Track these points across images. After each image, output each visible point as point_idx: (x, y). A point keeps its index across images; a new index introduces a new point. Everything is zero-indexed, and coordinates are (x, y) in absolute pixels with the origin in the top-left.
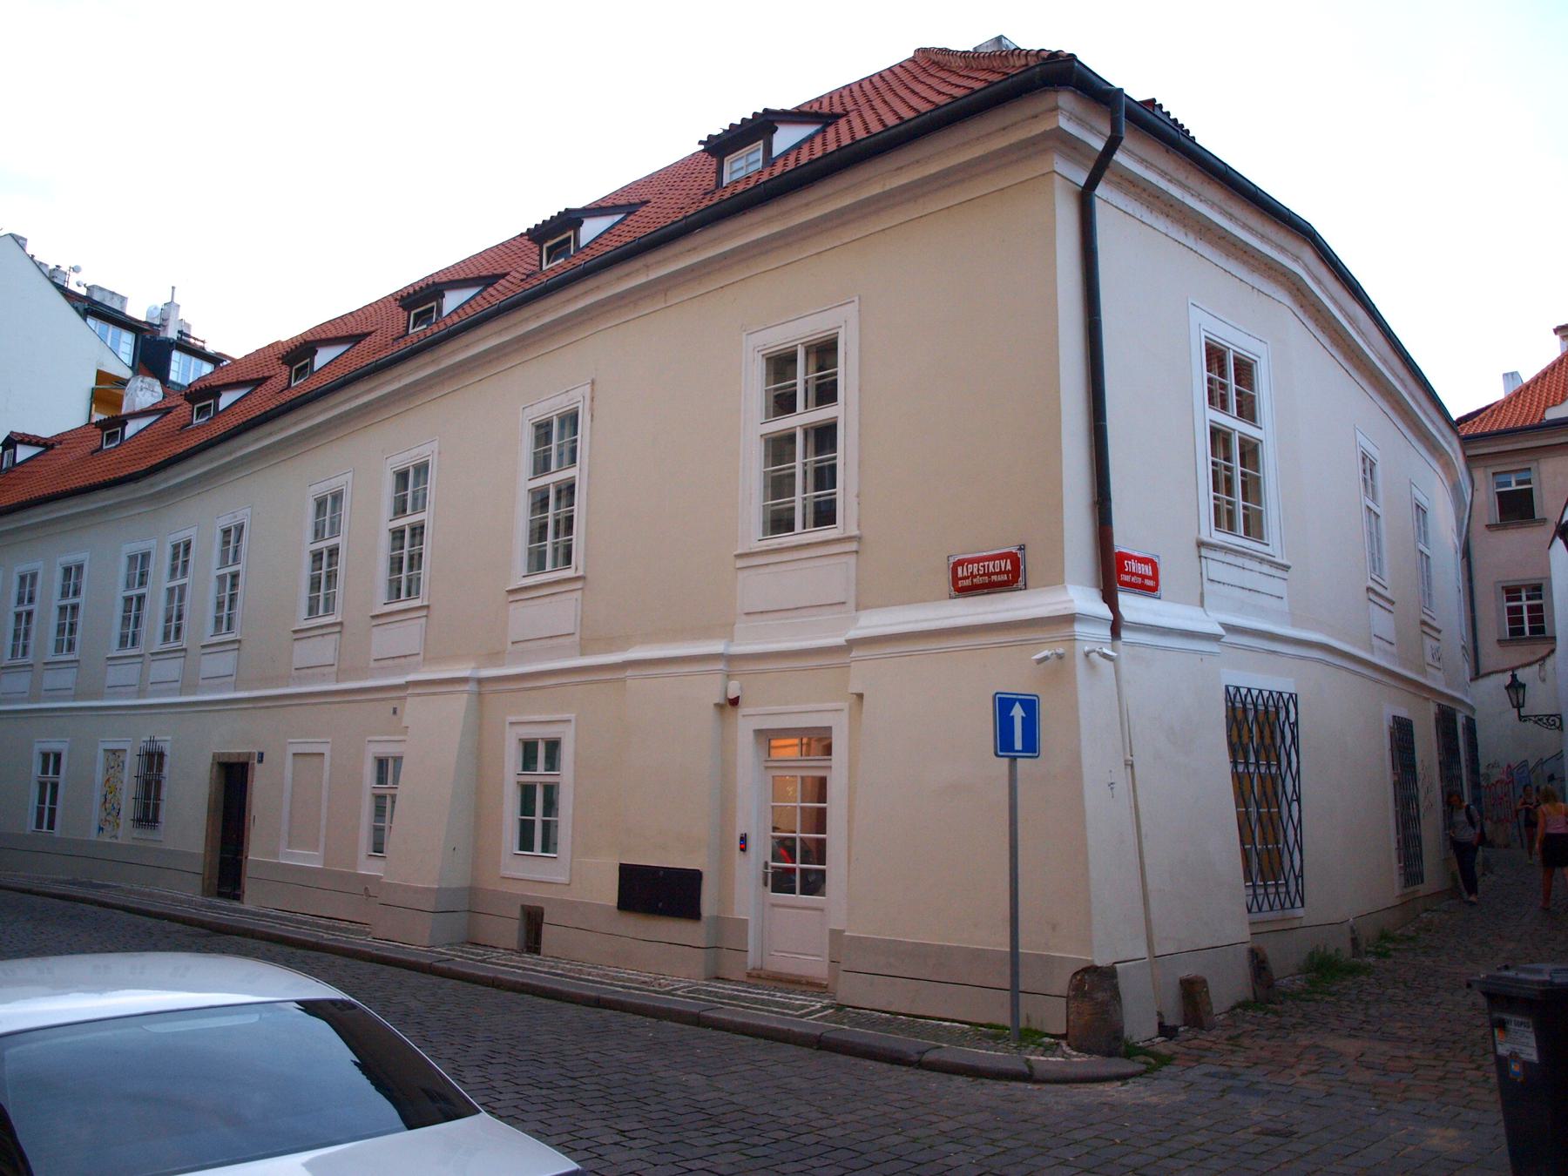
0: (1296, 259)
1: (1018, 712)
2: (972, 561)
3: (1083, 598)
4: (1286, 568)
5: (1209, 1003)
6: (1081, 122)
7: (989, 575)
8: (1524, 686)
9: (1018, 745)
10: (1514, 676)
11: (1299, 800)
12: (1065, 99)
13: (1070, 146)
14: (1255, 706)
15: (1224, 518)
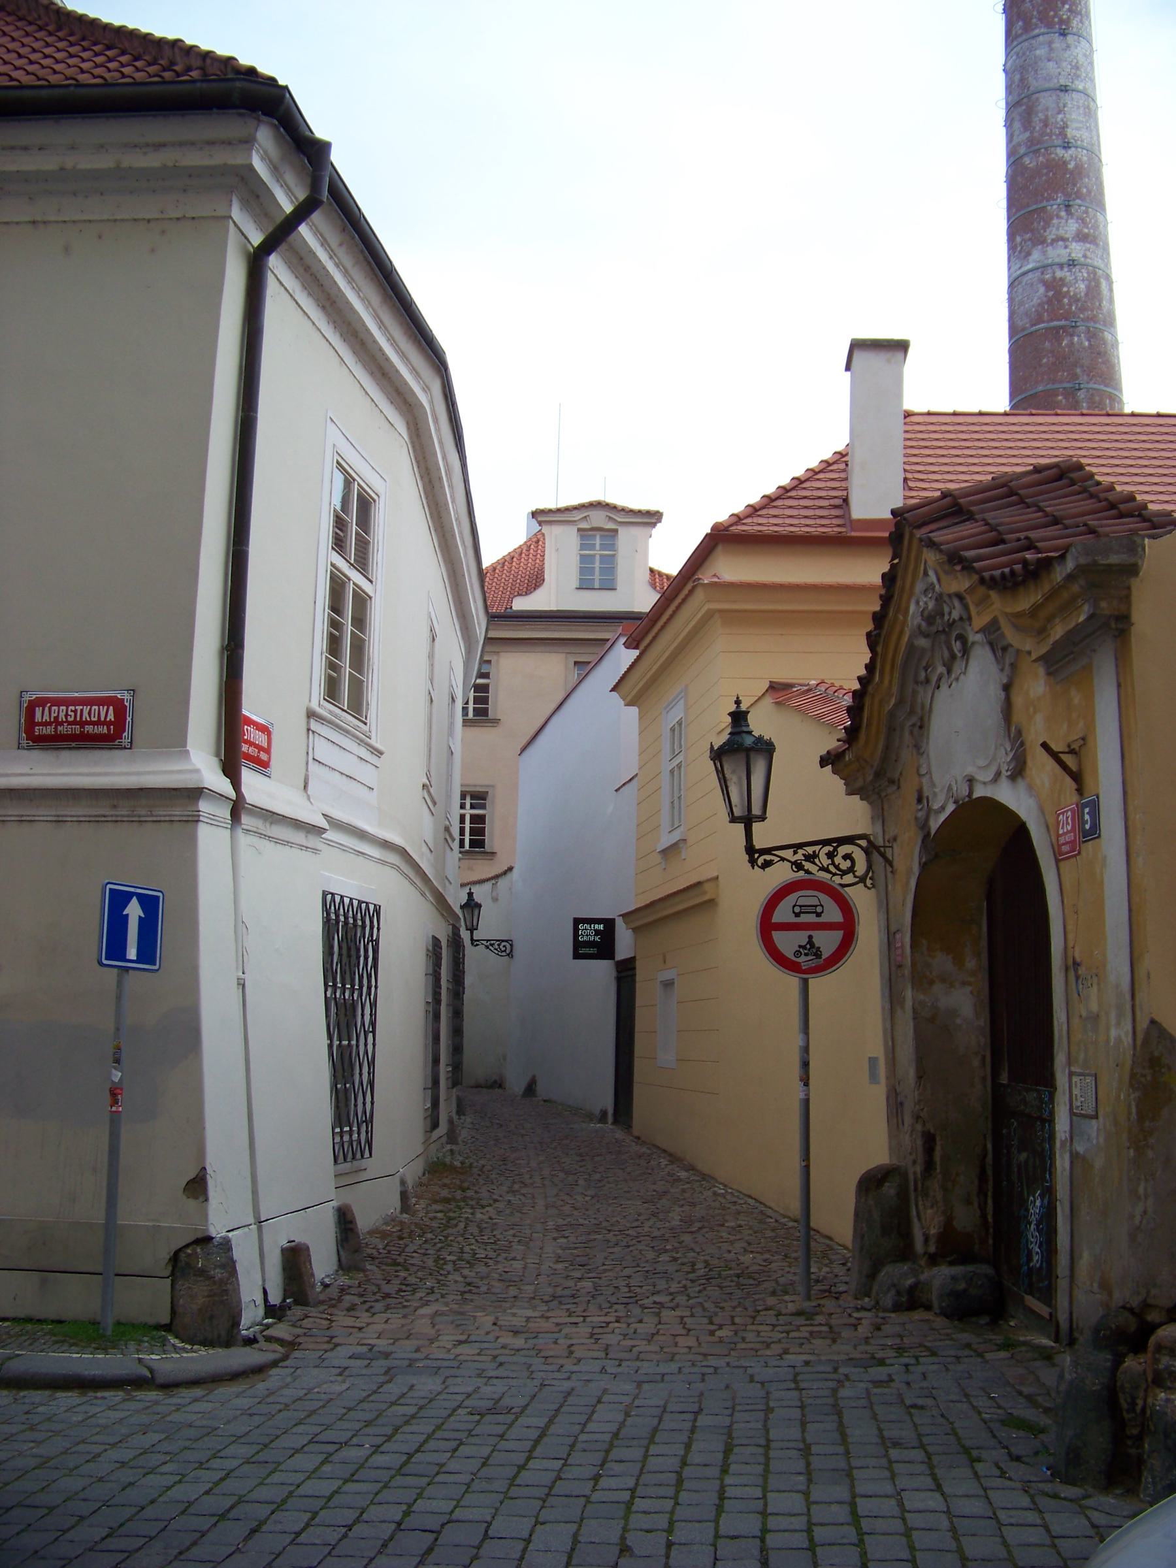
0: (426, 389)
1: (134, 911)
2: (58, 702)
3: (201, 764)
4: (379, 753)
5: (313, 1275)
6: (275, 170)
7: (83, 724)
8: (479, 906)
9: (132, 953)
10: (470, 894)
11: (374, 1032)
12: (265, 135)
13: (255, 196)
14: (346, 918)
15: (332, 691)
